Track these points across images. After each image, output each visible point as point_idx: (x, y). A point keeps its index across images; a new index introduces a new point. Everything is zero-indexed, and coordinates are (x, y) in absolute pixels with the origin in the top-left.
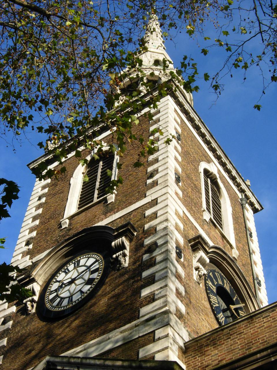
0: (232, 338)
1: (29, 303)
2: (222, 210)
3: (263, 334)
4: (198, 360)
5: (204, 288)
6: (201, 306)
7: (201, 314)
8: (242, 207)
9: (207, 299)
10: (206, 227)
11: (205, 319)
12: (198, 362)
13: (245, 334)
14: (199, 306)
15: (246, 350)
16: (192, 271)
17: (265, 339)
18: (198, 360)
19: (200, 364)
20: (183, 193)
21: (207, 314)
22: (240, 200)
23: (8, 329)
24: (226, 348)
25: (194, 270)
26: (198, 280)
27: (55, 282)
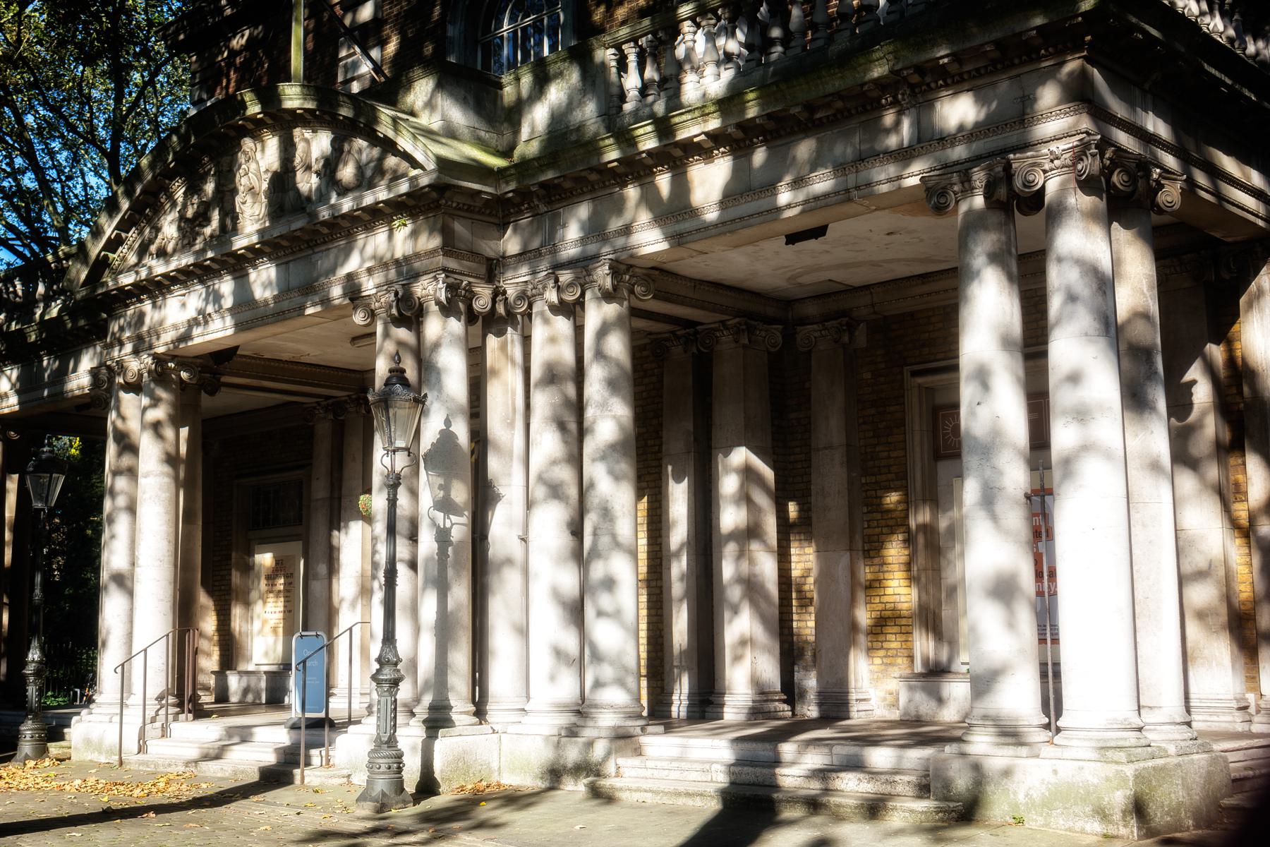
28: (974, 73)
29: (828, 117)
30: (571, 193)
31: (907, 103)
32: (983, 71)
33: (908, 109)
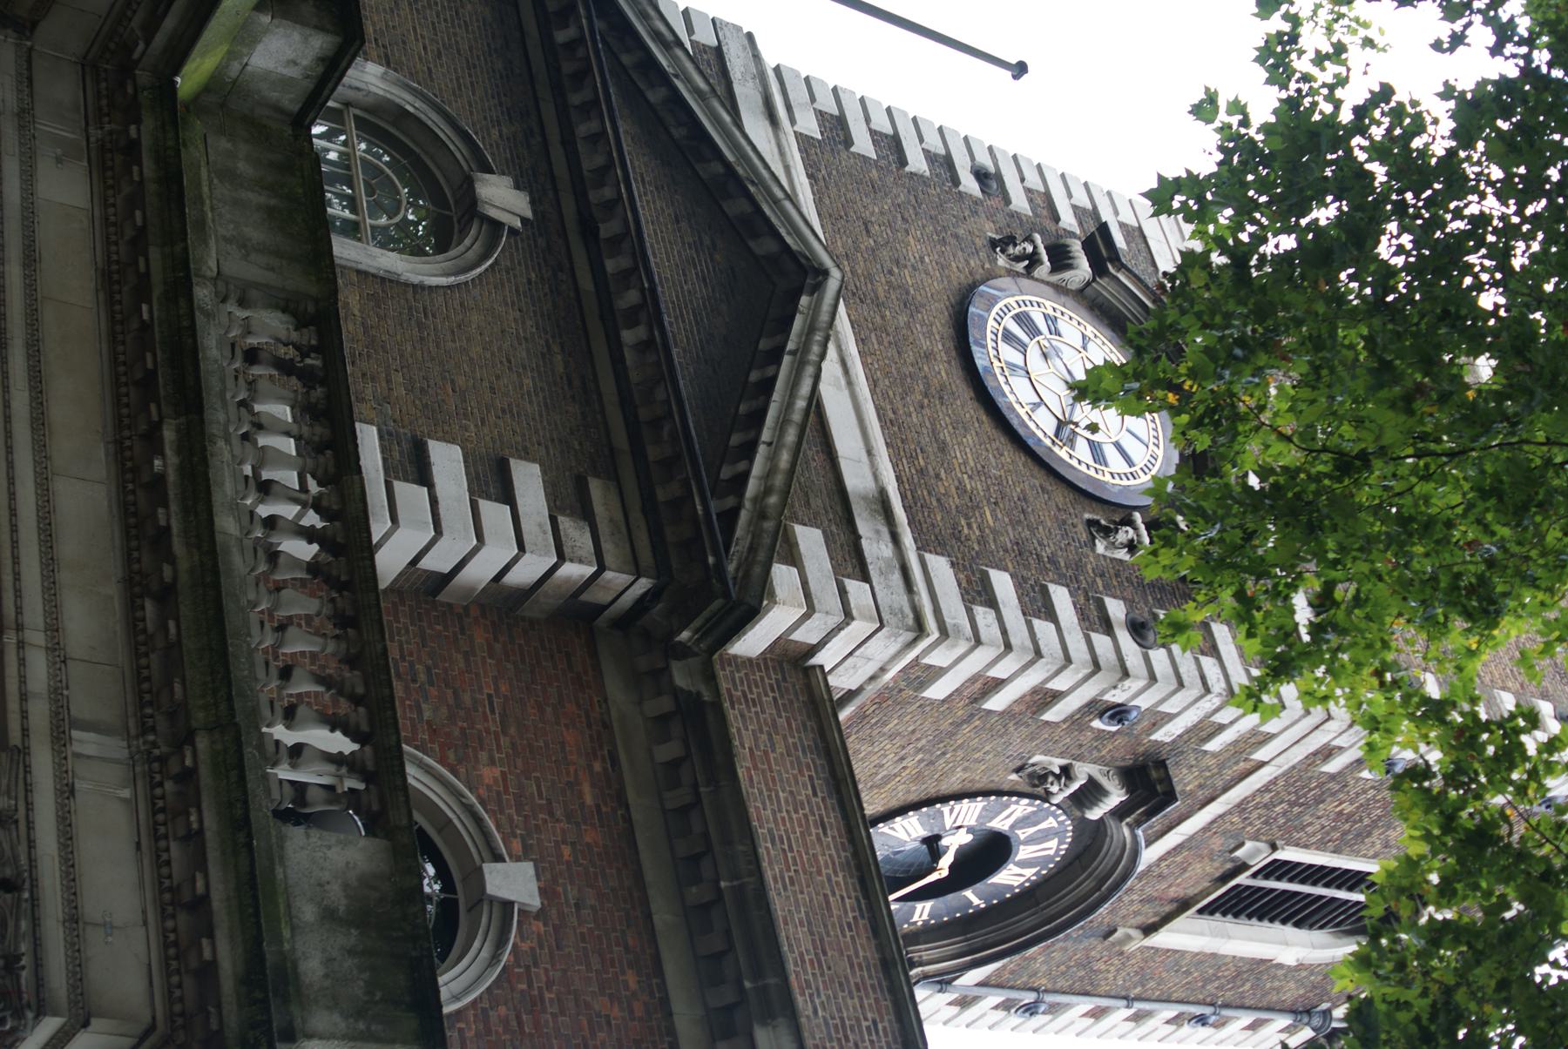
0: (814, 799)
1: (1030, 249)
2: (1289, 931)
3: (808, 886)
4: (766, 695)
5: (1006, 787)
6: (947, 763)
7: (920, 756)
8: (1301, 1012)
9: (968, 787)
10: (1217, 843)
11: (904, 768)
12: (759, 694)
13: (819, 839)
14: (944, 754)
15: (770, 831)
16: (1061, 755)
17: (867, 1024)
18: (766, 695)
19: (755, 696)
20: (1333, 777)
21: (918, 777)
22: (1325, 1006)
23: (956, 181)
24: (788, 779)
25: (1063, 762)
26: (1030, 769)
27: (1084, 336)
28: (165, 856)
29: (144, 620)
30: (112, 187)
31: (138, 747)
32: (165, 871)
33: (129, 747)
